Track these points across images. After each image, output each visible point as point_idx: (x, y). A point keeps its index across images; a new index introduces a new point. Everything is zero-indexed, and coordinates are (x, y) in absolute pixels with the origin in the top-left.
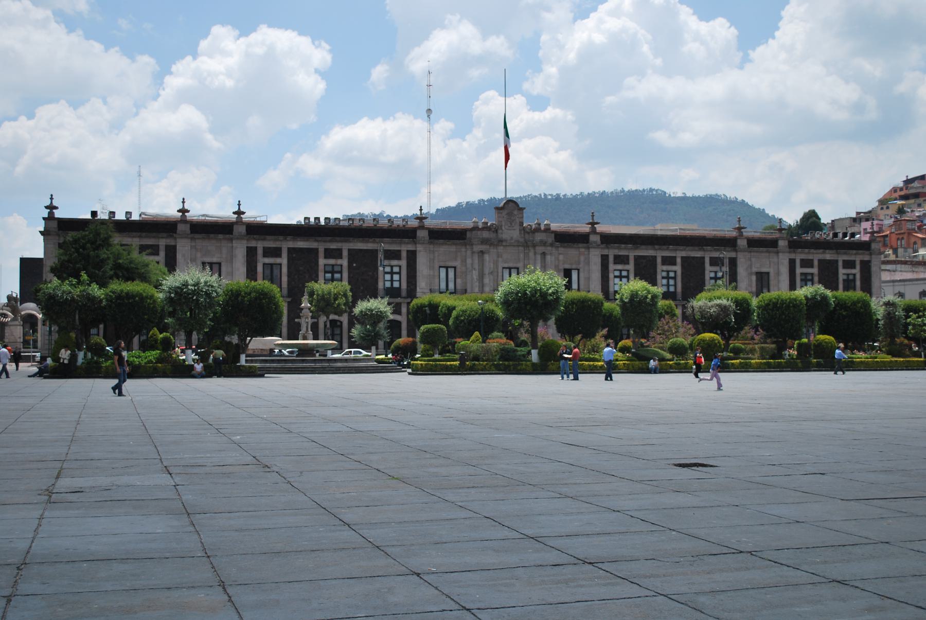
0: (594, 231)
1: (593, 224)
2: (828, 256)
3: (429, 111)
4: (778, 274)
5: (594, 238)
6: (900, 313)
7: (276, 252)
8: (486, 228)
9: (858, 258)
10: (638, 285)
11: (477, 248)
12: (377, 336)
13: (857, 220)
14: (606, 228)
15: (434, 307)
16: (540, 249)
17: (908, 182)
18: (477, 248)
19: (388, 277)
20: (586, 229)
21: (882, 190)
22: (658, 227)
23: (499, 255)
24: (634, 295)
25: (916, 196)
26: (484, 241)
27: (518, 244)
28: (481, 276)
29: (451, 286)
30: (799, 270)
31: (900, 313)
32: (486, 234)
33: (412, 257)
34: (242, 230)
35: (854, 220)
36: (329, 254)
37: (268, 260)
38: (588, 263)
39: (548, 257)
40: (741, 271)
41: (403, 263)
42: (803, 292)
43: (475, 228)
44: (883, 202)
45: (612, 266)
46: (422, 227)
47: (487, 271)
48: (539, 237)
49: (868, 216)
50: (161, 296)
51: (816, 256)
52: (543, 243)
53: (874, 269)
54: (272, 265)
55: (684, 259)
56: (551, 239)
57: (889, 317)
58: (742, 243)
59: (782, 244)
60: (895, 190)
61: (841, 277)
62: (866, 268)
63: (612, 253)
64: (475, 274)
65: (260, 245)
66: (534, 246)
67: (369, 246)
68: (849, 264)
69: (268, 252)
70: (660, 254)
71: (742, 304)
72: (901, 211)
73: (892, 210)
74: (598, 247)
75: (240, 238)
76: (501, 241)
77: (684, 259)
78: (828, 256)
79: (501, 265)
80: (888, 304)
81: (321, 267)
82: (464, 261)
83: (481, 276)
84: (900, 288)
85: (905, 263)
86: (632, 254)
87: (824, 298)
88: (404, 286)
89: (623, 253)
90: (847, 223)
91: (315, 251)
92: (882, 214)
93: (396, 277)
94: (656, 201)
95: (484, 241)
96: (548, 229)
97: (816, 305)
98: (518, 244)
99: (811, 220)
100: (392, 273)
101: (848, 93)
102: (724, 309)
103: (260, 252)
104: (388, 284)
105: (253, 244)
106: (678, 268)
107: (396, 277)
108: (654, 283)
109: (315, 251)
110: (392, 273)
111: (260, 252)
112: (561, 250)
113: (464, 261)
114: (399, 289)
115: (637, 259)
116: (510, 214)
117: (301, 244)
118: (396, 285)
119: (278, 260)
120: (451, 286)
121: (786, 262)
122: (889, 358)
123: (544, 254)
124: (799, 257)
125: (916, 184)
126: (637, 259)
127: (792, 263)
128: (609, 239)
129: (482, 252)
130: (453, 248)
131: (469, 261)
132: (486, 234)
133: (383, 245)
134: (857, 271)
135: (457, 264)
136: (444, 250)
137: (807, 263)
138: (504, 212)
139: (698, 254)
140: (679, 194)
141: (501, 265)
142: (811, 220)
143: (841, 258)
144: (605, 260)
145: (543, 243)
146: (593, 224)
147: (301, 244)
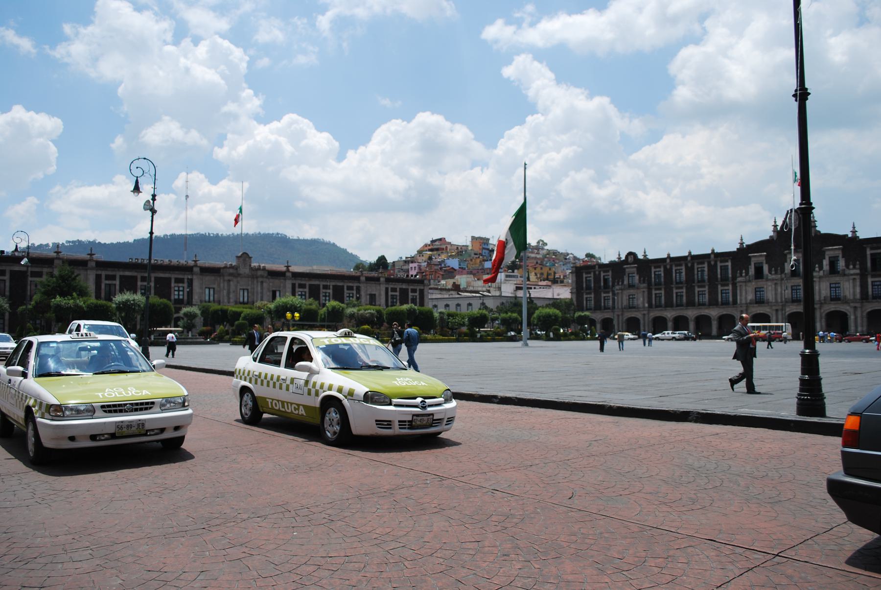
0: (288, 270)
1: (288, 267)
2: (404, 286)
3: (187, 196)
4: (380, 295)
5: (288, 274)
6: (445, 317)
7: (113, 278)
8: (231, 267)
9: (418, 288)
10: (333, 303)
11: (227, 278)
12: (194, 326)
13: (407, 262)
14: (294, 269)
15: (224, 312)
16: (260, 280)
17: (433, 241)
18: (227, 278)
19: (176, 293)
20: (284, 269)
21: (419, 246)
22: (315, 267)
23: (238, 282)
24: (334, 308)
25: (437, 250)
26: (231, 275)
27: (248, 277)
28: (229, 293)
29: (212, 298)
30: (390, 293)
31: (445, 317)
32: (231, 271)
33: (190, 283)
34: (94, 264)
35: (405, 262)
36: (143, 279)
37: (107, 282)
38: (285, 287)
39: (265, 284)
40: (363, 293)
41: (186, 285)
42: (405, 307)
43: (225, 267)
44: (420, 252)
45: (297, 289)
46: (196, 266)
47: (231, 290)
48: (260, 273)
49: (412, 260)
50: (114, 305)
51: (399, 286)
52: (262, 276)
53: (425, 293)
54: (110, 285)
55: (334, 286)
56: (266, 274)
57: (442, 319)
58: (363, 279)
59: (382, 279)
60: (426, 245)
61: (410, 297)
62: (422, 292)
63: (297, 282)
64: (225, 292)
65: (103, 273)
66: (257, 278)
67: (167, 275)
68: (414, 291)
69: (108, 277)
70: (322, 284)
71: (378, 312)
72: (430, 258)
73: (425, 258)
74: (290, 279)
75: (92, 269)
76: (239, 275)
77: (334, 286)
78: (404, 286)
79: (239, 287)
80: (440, 313)
81: (139, 286)
82: (219, 285)
83: (229, 293)
84: (435, 303)
85: (437, 289)
86: (308, 283)
87: (414, 310)
88: (186, 298)
89: (303, 282)
90: (402, 263)
91: (135, 278)
92: (420, 259)
93: (181, 293)
94: (282, 241)
95: (231, 275)
96: (264, 269)
97: (411, 312)
98: (248, 277)
99: (382, 260)
100: (179, 291)
101: (401, 184)
102: (372, 314)
103: (103, 277)
104: (176, 297)
105: (99, 272)
106: (331, 291)
107: (181, 293)
108: (343, 303)
109: (135, 278)
110: (179, 291)
111: (103, 277)
112: (271, 280)
113: (219, 285)
114: (183, 300)
115: (310, 286)
116: (244, 260)
117: (127, 273)
118: (181, 297)
119: (114, 282)
120: (212, 298)
121: (384, 289)
122: (441, 337)
123: (262, 282)
124: (390, 286)
125: (437, 243)
126: (310, 286)
127: (387, 289)
128: (296, 275)
129: (229, 281)
130: (213, 278)
131: (222, 285)
132: (231, 271)
133: (173, 276)
134: (417, 294)
135: (215, 286)
136: (208, 278)
137: (394, 290)
138: (241, 259)
139: (341, 284)
140: (295, 238)
141: (239, 287)
142: (382, 260)
143: (410, 288)
144: (294, 286)
145: (262, 276)
146: (288, 267)
147: (127, 273)
